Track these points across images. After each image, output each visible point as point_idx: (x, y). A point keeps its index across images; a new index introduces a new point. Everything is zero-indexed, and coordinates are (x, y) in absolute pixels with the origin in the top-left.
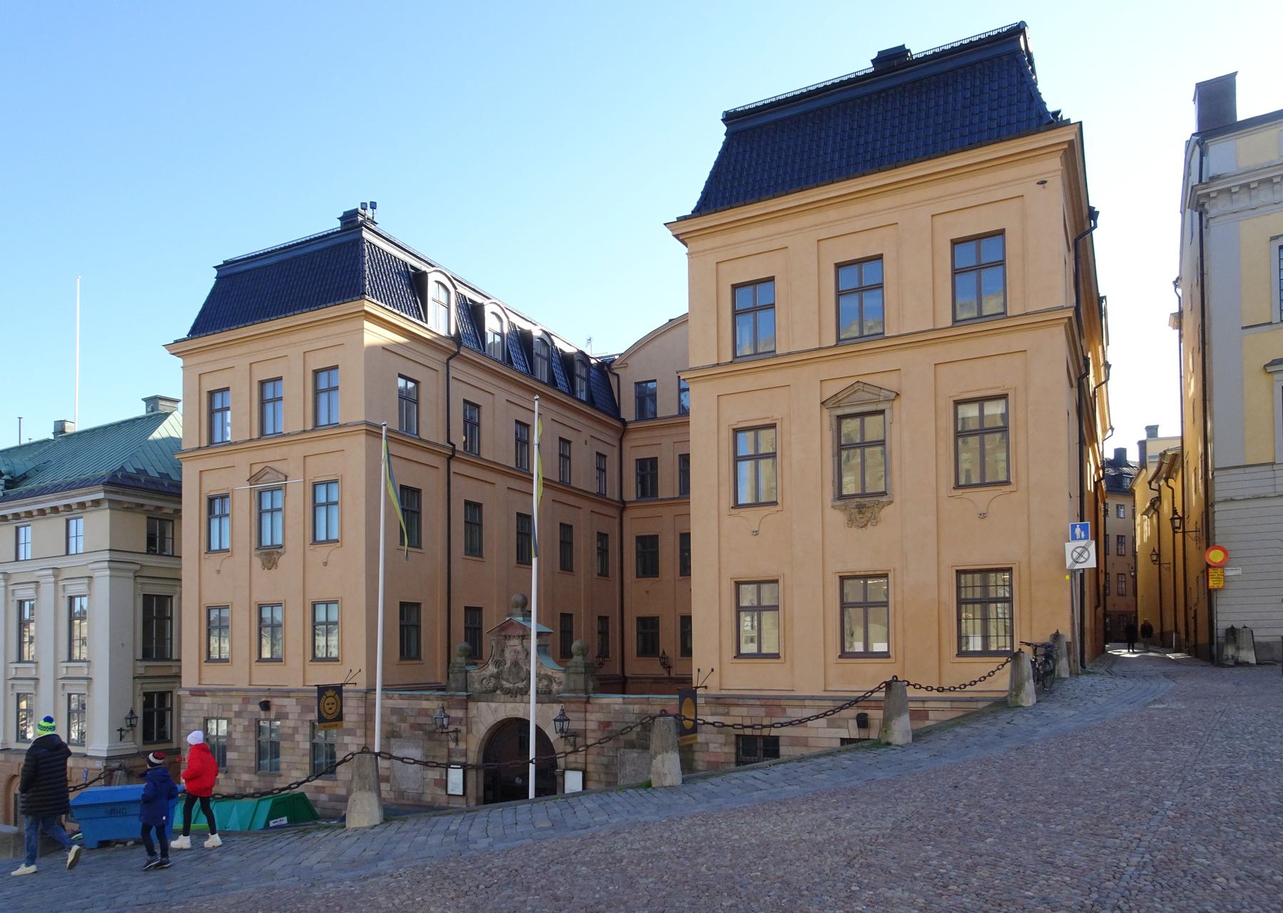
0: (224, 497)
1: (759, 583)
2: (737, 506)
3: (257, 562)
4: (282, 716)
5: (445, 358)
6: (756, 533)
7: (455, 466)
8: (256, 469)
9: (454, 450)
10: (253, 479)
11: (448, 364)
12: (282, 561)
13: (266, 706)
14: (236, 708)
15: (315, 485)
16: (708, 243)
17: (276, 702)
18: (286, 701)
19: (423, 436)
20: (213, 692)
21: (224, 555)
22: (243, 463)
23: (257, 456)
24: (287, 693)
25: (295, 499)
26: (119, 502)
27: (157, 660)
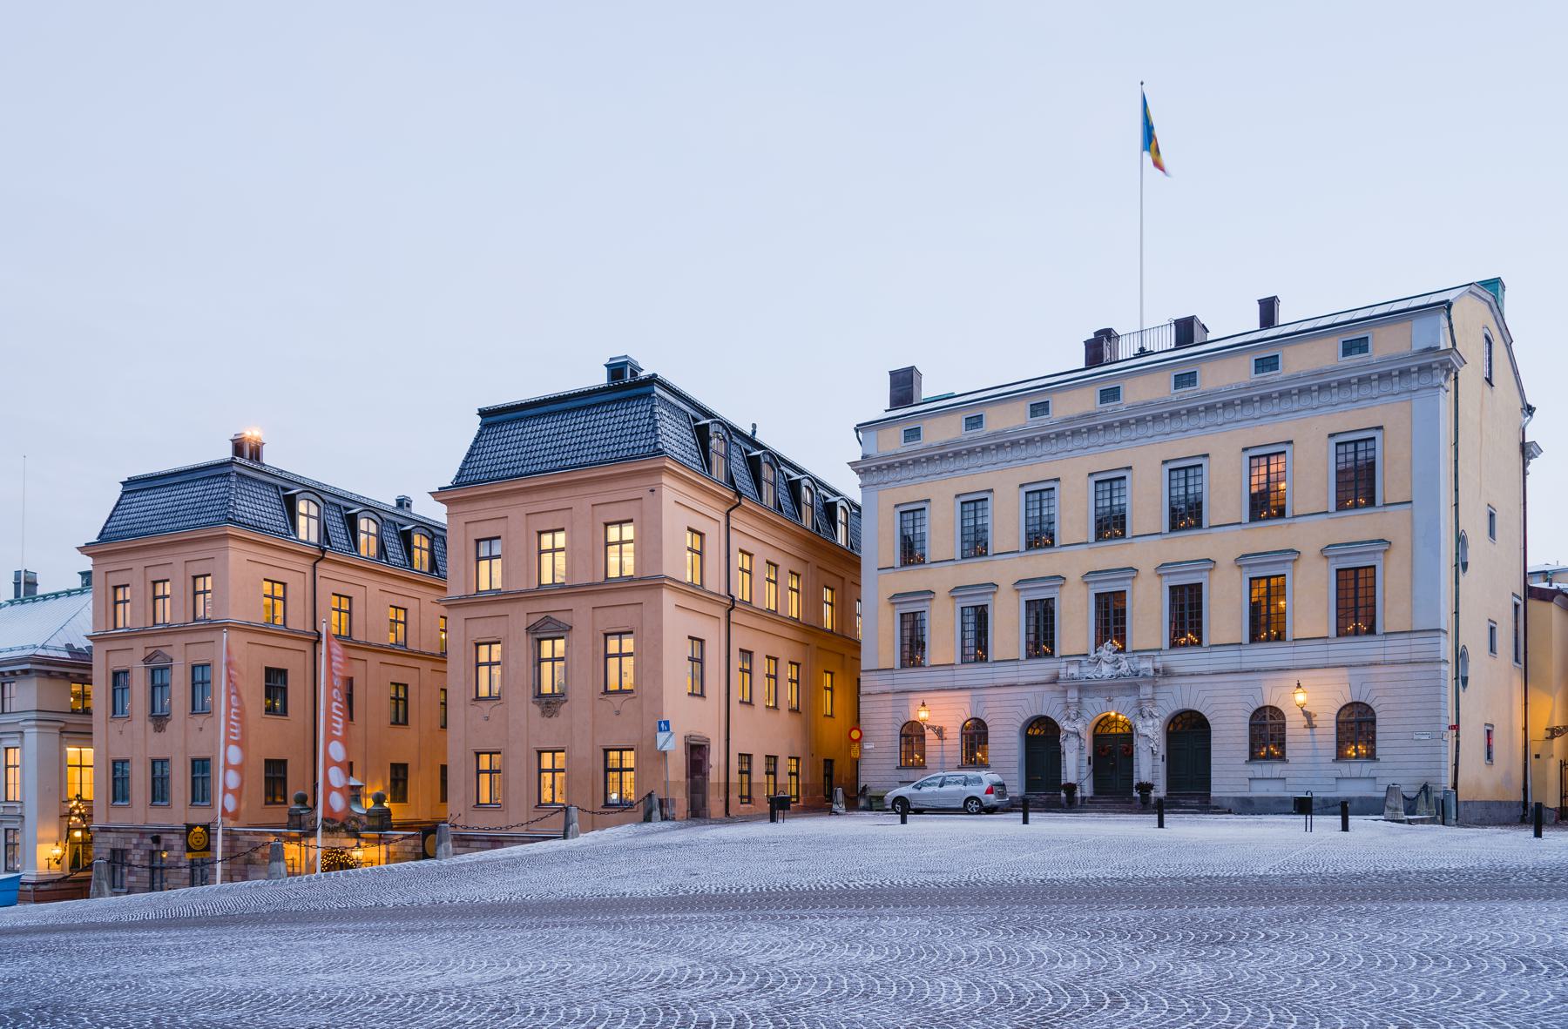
0: (126, 672)
1: (491, 754)
2: (606, 692)
3: (150, 726)
4: (168, 848)
5: (725, 509)
6: (487, 719)
7: (735, 616)
8: (150, 651)
9: (733, 601)
10: (147, 660)
11: (728, 514)
12: (169, 726)
13: (156, 840)
14: (135, 841)
15: (194, 667)
16: (460, 508)
17: (164, 836)
18: (172, 837)
19: (708, 588)
20: (117, 830)
21: (624, 697)
22: (140, 648)
23: (151, 642)
24: (172, 831)
25: (179, 680)
26: (48, 672)
27: (721, 822)
